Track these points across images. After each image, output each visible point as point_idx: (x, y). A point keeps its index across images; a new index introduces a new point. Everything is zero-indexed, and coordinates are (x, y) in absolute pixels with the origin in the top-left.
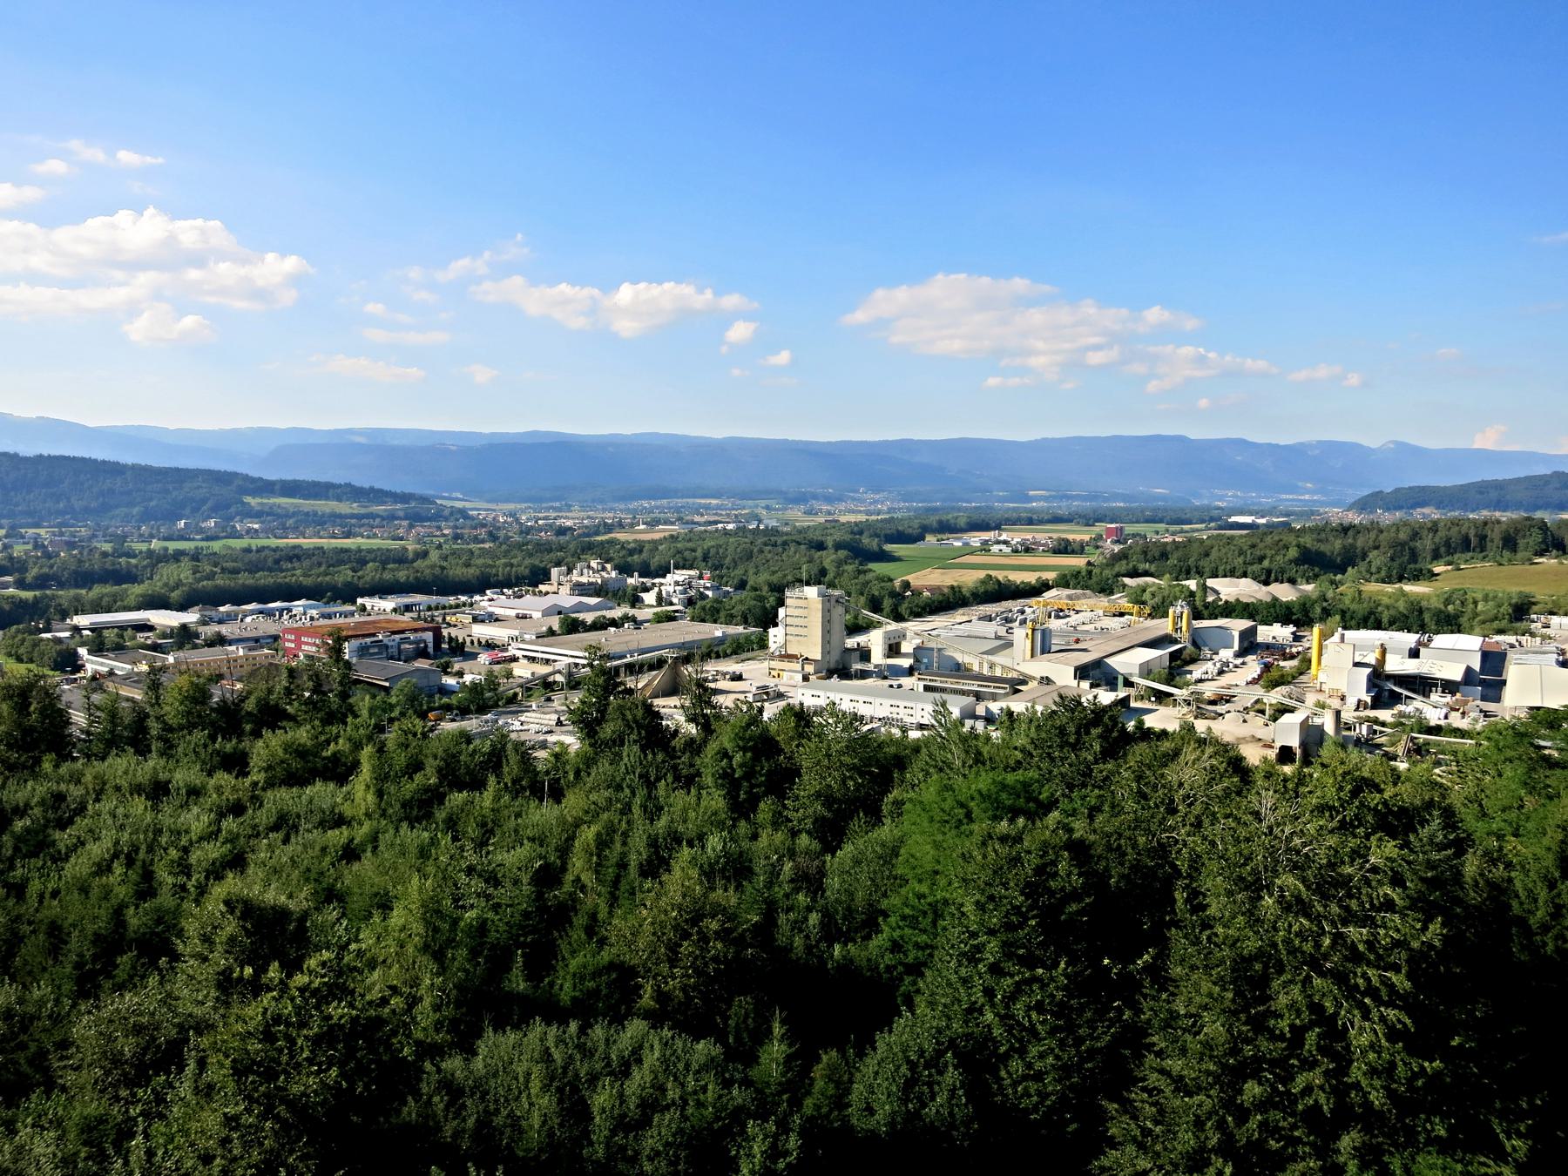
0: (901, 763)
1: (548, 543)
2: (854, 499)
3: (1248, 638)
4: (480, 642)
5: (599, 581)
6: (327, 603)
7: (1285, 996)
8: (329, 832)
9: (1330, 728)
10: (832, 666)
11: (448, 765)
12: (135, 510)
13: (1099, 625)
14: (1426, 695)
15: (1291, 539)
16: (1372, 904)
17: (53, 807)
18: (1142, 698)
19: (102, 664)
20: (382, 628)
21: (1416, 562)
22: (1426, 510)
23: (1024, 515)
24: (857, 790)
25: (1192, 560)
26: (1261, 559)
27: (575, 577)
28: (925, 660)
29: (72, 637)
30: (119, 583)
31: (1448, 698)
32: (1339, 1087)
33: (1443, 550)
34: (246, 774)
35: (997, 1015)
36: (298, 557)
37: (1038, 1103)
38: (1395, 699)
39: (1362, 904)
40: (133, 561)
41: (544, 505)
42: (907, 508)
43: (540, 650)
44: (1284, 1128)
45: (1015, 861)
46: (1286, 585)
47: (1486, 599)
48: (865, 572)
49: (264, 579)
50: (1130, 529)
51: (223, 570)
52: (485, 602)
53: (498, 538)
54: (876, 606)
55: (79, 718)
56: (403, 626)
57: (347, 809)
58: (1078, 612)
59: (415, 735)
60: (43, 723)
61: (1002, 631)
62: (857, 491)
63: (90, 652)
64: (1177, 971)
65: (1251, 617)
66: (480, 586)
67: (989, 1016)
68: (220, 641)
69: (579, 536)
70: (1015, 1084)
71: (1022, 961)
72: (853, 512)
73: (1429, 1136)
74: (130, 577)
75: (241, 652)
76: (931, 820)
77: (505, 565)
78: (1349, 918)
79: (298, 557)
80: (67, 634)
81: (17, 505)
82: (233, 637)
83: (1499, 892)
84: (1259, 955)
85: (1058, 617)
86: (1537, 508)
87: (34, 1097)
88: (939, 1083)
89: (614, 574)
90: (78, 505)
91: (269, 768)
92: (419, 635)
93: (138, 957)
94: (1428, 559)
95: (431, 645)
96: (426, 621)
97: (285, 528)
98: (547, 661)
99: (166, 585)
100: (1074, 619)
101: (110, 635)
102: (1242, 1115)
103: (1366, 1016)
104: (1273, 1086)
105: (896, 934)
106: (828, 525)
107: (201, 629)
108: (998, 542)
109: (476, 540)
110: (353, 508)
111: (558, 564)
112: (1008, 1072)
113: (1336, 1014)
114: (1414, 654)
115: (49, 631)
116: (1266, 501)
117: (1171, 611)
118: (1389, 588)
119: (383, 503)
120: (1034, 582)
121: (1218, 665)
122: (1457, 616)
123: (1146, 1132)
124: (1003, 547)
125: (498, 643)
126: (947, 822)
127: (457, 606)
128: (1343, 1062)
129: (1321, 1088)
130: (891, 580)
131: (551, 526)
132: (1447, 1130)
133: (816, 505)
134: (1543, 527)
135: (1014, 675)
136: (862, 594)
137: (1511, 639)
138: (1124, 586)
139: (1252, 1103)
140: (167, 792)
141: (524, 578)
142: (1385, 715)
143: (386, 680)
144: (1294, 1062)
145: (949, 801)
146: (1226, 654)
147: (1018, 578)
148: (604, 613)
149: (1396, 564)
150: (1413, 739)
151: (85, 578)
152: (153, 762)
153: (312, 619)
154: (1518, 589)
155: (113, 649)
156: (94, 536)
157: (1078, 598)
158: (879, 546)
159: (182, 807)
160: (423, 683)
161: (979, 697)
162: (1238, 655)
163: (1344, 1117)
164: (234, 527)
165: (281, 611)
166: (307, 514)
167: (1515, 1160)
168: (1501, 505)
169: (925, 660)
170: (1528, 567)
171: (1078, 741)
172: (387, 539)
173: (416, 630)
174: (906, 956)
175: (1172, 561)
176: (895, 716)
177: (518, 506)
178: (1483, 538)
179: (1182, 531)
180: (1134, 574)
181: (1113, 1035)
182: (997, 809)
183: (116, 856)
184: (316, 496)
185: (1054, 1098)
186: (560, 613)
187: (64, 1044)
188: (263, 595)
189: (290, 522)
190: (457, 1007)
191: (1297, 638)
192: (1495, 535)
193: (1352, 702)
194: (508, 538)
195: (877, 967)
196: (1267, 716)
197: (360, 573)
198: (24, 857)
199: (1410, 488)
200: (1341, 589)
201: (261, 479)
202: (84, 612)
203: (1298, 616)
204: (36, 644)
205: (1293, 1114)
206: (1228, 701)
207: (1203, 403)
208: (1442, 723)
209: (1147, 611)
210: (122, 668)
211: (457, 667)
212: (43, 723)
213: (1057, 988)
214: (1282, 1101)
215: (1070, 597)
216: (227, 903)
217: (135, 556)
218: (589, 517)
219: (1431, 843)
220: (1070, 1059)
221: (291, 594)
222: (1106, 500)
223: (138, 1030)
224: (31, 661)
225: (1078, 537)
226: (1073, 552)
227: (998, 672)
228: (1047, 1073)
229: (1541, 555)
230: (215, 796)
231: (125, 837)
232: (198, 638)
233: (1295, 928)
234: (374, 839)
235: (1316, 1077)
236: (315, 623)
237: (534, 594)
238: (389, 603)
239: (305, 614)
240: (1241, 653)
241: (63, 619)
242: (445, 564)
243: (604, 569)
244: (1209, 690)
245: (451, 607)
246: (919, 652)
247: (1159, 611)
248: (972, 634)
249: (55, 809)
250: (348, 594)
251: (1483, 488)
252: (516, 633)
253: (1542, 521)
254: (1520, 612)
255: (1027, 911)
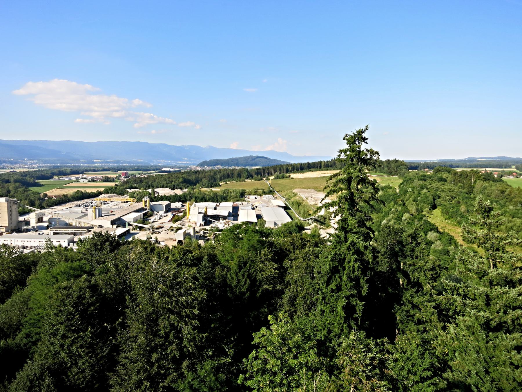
0: (35, 264)
2: (22, 163)
3: (168, 206)
7: (163, 323)
9: (192, 234)
10: (13, 228)
13: (119, 206)
14: (219, 221)
15: (180, 175)
16: (186, 289)
18: (134, 229)
21: (215, 182)
22: (218, 166)
23: (92, 168)
24: (16, 276)
25: (150, 183)
26: (172, 182)
28: (53, 223)
31: (224, 221)
32: (181, 349)
33: (222, 178)
35: (65, 353)
37: (83, 381)
38: (211, 222)
39: (183, 290)
42: (46, 166)
44: (166, 365)
45: (69, 296)
46: (179, 190)
47: (234, 191)
48: (27, 191)
50: (130, 173)
54: (32, 205)
58: (112, 202)
61: (84, 210)
62: (24, 160)
64: (129, 323)
65: (169, 200)
67: (63, 354)
70: (74, 376)
71: (74, 331)
72: (22, 168)
73: (207, 356)
76: (42, 284)
78: (181, 295)
83: (224, 278)
84: (154, 312)
85: (105, 204)
86: (246, 166)
88: (43, 385)
94: (219, 180)
100: (111, 204)
102: (152, 365)
103: (186, 325)
104: (162, 354)
105: (27, 331)
106: (11, 173)
108: (82, 178)
112: (72, 373)
113: (178, 325)
114: (215, 209)
116: (174, 164)
117: (143, 200)
118: (208, 190)
120: (96, 192)
121: (159, 216)
122: (226, 197)
123: (123, 380)
124: (84, 180)
126: (48, 284)
128: (181, 339)
129: (175, 350)
130: (39, 193)
132: (212, 352)
133: (6, 165)
134: (247, 170)
135: (89, 225)
136: (26, 199)
137: (240, 203)
138: (128, 192)
139: (155, 360)
142: (208, 228)
144: (167, 344)
145: (49, 277)
146: (162, 213)
147: (89, 191)
149: (210, 182)
150: (215, 234)
154: (242, 188)
157: (112, 197)
158: (34, 180)
161: (75, 234)
162: (165, 213)
163: (183, 357)
167: (231, 356)
168: (237, 165)
169: (53, 223)
170: (244, 182)
171: (101, 247)
174: (32, 338)
175: (144, 183)
176: (41, 245)
178: (232, 174)
179: (147, 173)
180: (131, 188)
181: (109, 350)
182: (68, 277)
185: (89, 377)
191: (183, 206)
192: (236, 174)
193: (198, 224)
195: (20, 345)
196: (174, 231)
199: (214, 160)
200: (195, 190)
203: (182, 199)
205: (168, 360)
206: (162, 228)
207: (153, 132)
208: (223, 228)
209: (136, 200)
213: (88, 338)
214: (164, 357)
215: (109, 197)
219: (205, 267)
220: (94, 362)
222: (122, 163)
225: (112, 176)
226: (110, 181)
227: (83, 225)
228: (86, 369)
229: (247, 179)
233: (164, 301)
235: (174, 347)
240: (166, 212)
244: (156, 225)
246: (50, 221)
247: (139, 200)
248: (74, 212)
251: (246, 158)
253: (247, 169)
254: (242, 195)
255: (75, 313)
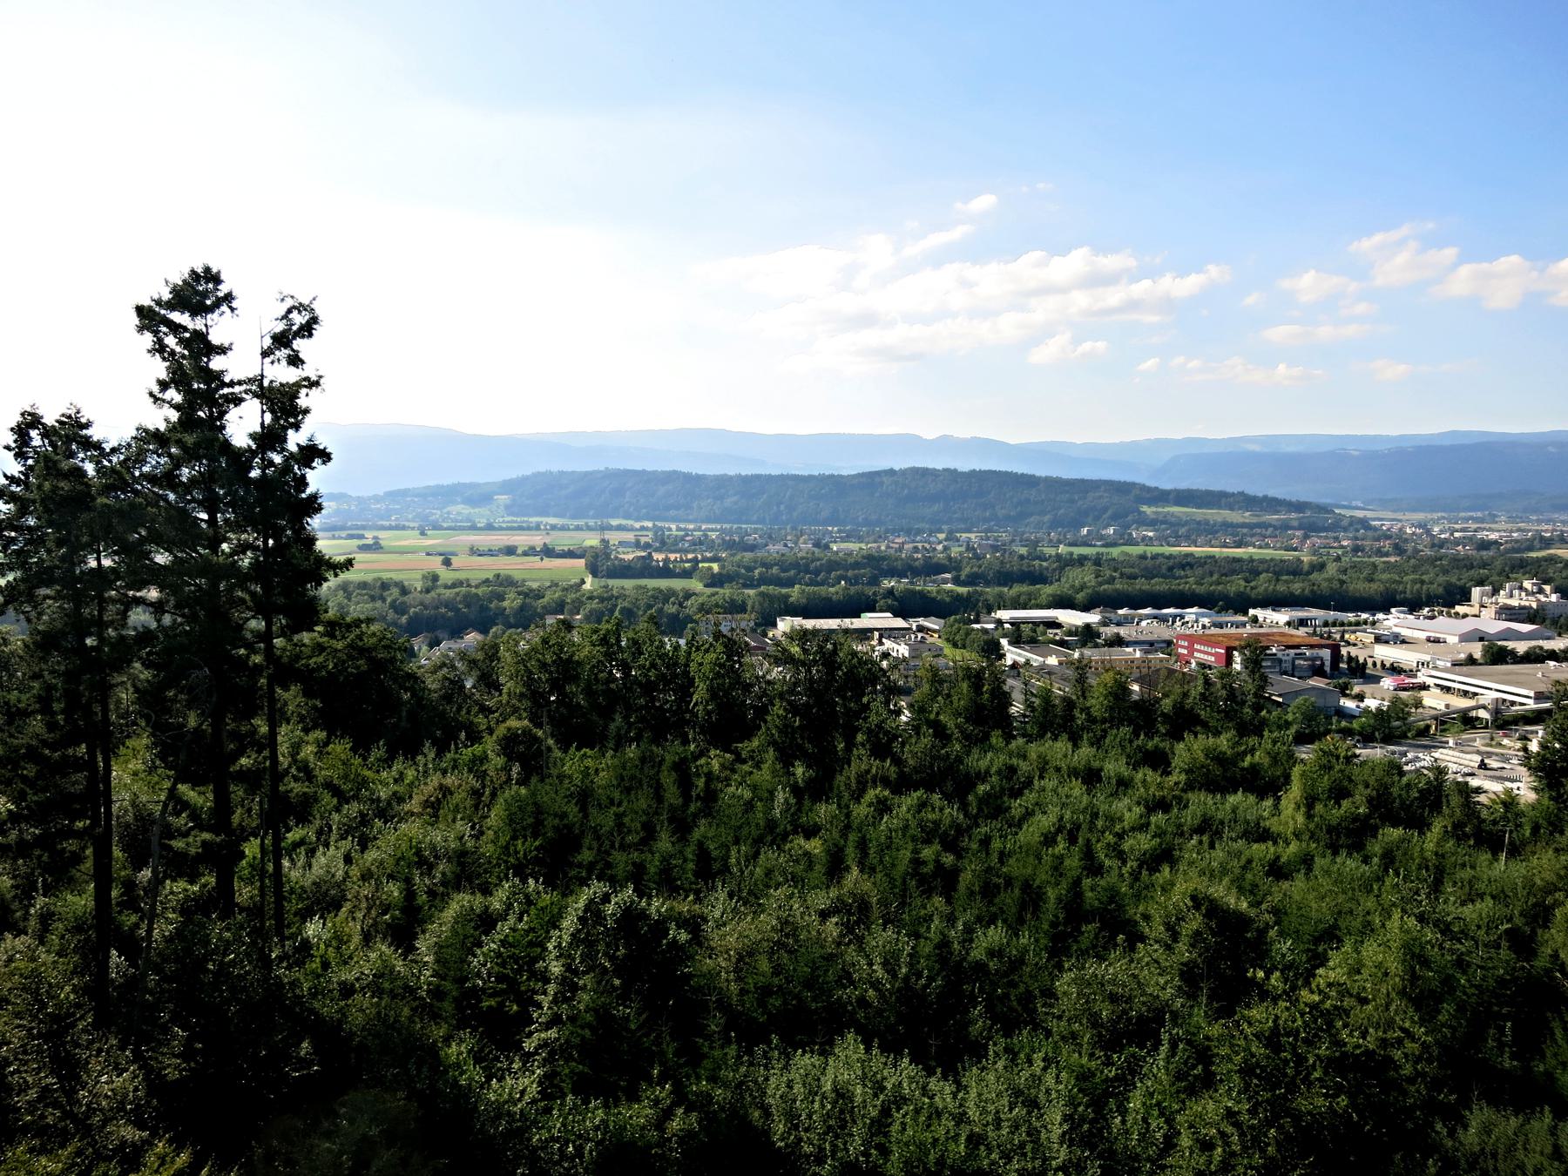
1: (1467, 557)
4: (1383, 665)
5: (1534, 605)
6: (1219, 612)
8: (1255, 846)
11: (1379, 795)
12: (1047, 518)
17: (1007, 778)
19: (1020, 655)
20: (1277, 642)
27: (1502, 599)
29: (996, 628)
30: (1034, 583)
34: (1169, 773)
36: (1191, 566)
40: (1045, 564)
41: (1462, 514)
43: (1458, 680)
49: (1159, 585)
51: (1122, 575)
52: (1394, 621)
53: (1406, 551)
55: (1016, 708)
56: (1297, 641)
57: (1273, 825)
59: (1338, 757)
60: (992, 702)
63: (1010, 643)
66: (1385, 604)
68: (1118, 641)
69: (1507, 551)
74: (1039, 578)
75: (1138, 654)
77: (1414, 582)
79: (1191, 566)
80: (992, 626)
81: (955, 513)
82: (1130, 639)
87: (1025, 1032)
89: (1554, 598)
90: (1001, 513)
91: (1188, 772)
92: (1315, 651)
93: (1101, 930)
95: (1328, 663)
96: (1322, 637)
97: (1177, 537)
98: (1465, 693)
99: (1073, 586)
101: (1025, 629)
107: (1102, 629)
109: (1380, 553)
110: (1246, 517)
111: (1481, 583)
115: (978, 622)
119: (1277, 512)
125: (1405, 667)
127: (1358, 624)
131: (1471, 539)
140: (1100, 780)
141: (1437, 597)
143: (1280, 696)
148: (1541, 643)
151: (1006, 578)
152: (1086, 752)
153: (1204, 627)
155: (1028, 642)
156: (1013, 541)
159: (1112, 795)
160: (1320, 703)
164: (1131, 534)
165: (1175, 617)
166: (1199, 523)
171: (629, 846)
172: (1280, 549)
173: (1312, 647)
177: (1429, 516)
183: (1059, 830)
184: (1209, 505)
186: (1481, 639)
187: (1049, 994)
188: (1158, 601)
189: (1182, 531)
190: (1440, 1067)
194: (1417, 551)
197: (1252, 584)
198: (987, 818)
201: (1156, 488)
202: (1005, 608)
204: (968, 633)
210: (1036, 660)
211: (1356, 689)
212: (992, 702)
216: (1193, 898)
217: (1046, 560)
218: (1519, 530)
221: (1184, 601)
223: (1113, 998)
224: (964, 647)
230: (1142, 790)
231: (1068, 815)
232: (1099, 638)
234: (1307, 861)
236: (1207, 632)
237: (1449, 615)
238: (1281, 617)
239: (1197, 621)
241: (989, 613)
242: (1344, 578)
243: (1541, 591)
245: (1350, 624)
249: (1009, 779)
250: (1241, 604)
252: (1427, 658)
